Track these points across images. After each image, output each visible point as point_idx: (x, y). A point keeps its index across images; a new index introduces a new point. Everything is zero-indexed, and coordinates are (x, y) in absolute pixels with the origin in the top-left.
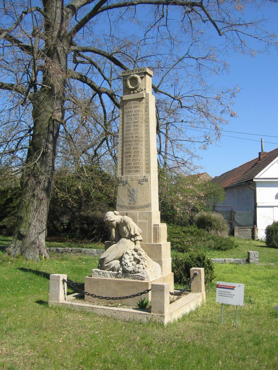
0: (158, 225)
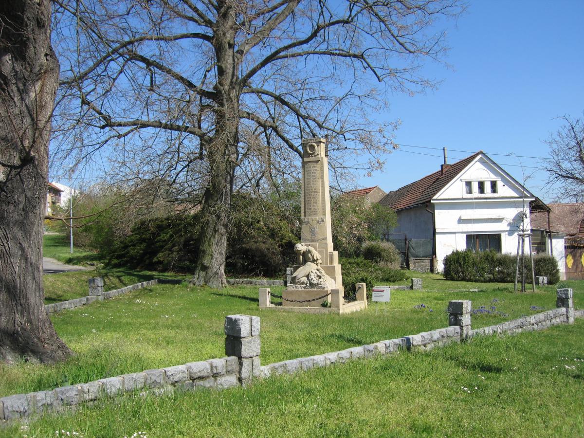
0: (332, 252)
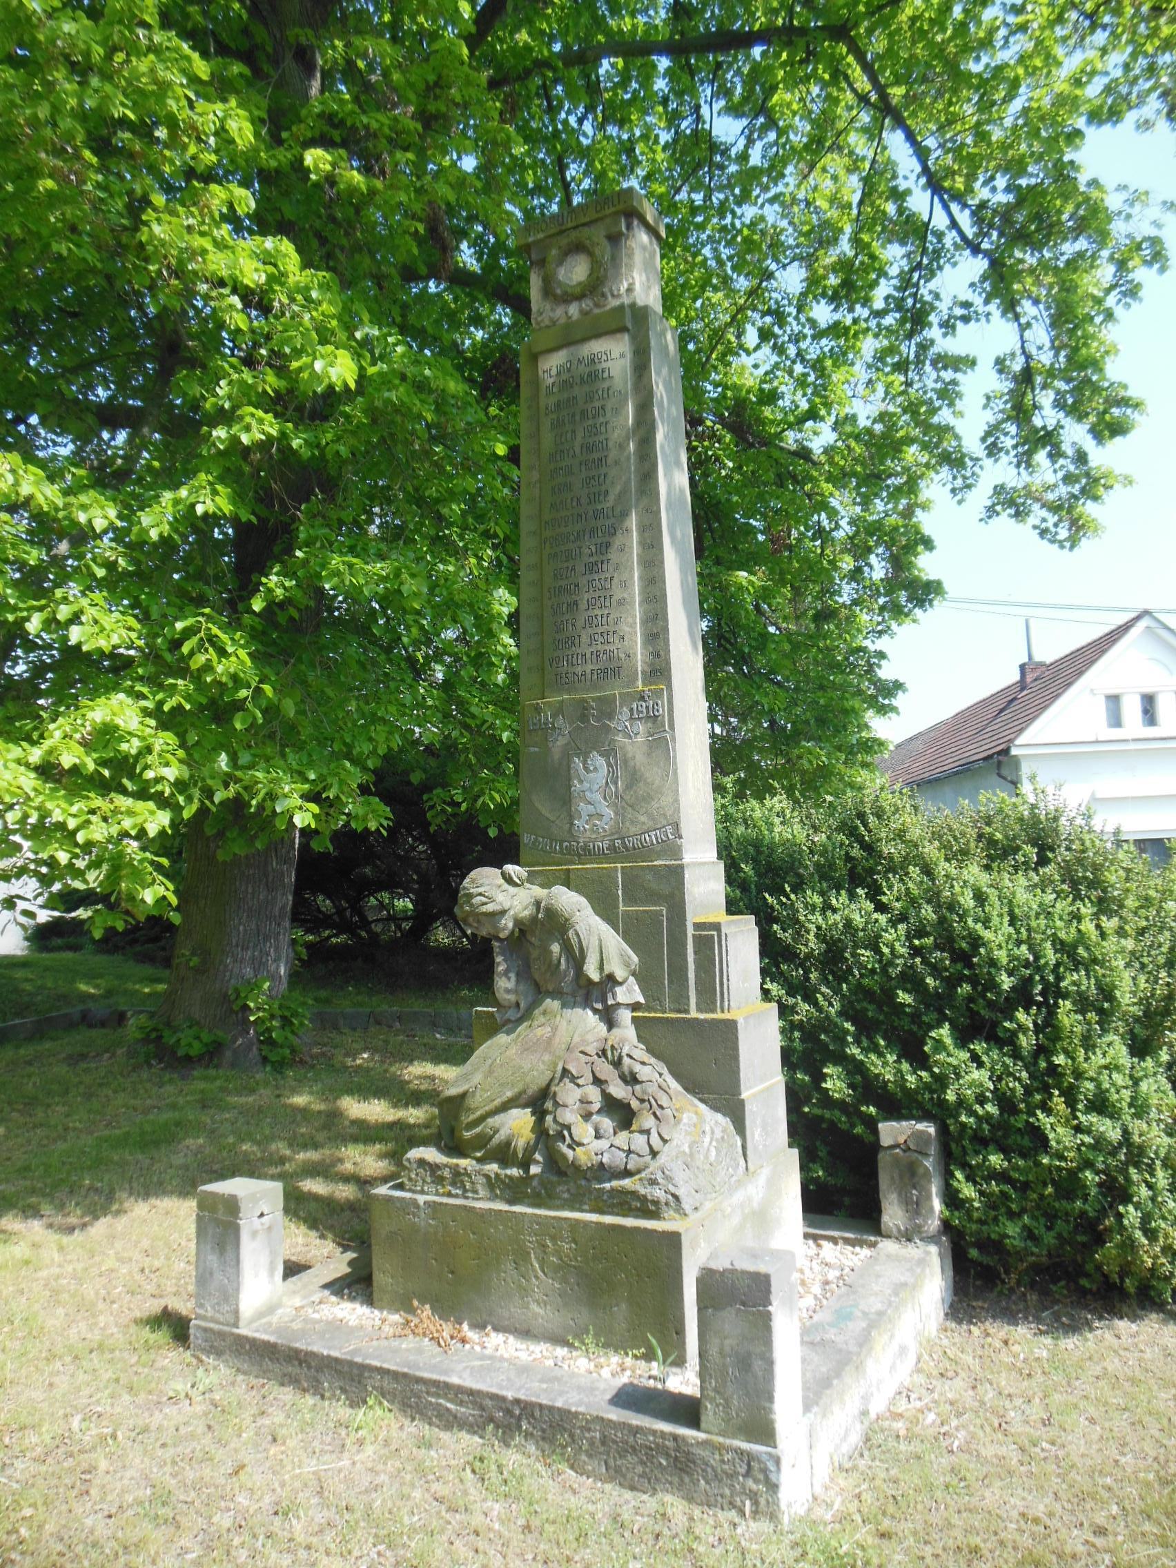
0: (717, 927)
